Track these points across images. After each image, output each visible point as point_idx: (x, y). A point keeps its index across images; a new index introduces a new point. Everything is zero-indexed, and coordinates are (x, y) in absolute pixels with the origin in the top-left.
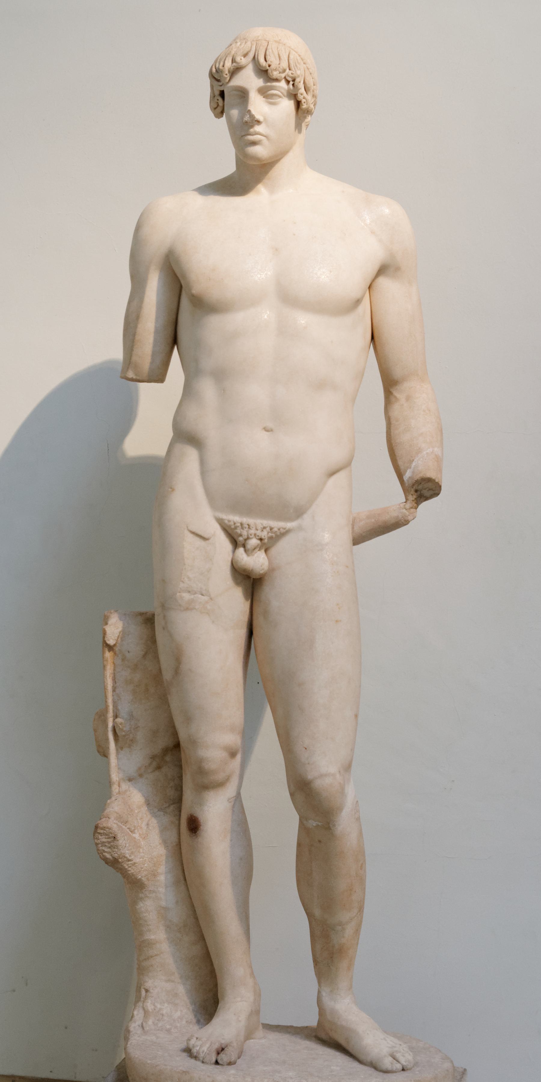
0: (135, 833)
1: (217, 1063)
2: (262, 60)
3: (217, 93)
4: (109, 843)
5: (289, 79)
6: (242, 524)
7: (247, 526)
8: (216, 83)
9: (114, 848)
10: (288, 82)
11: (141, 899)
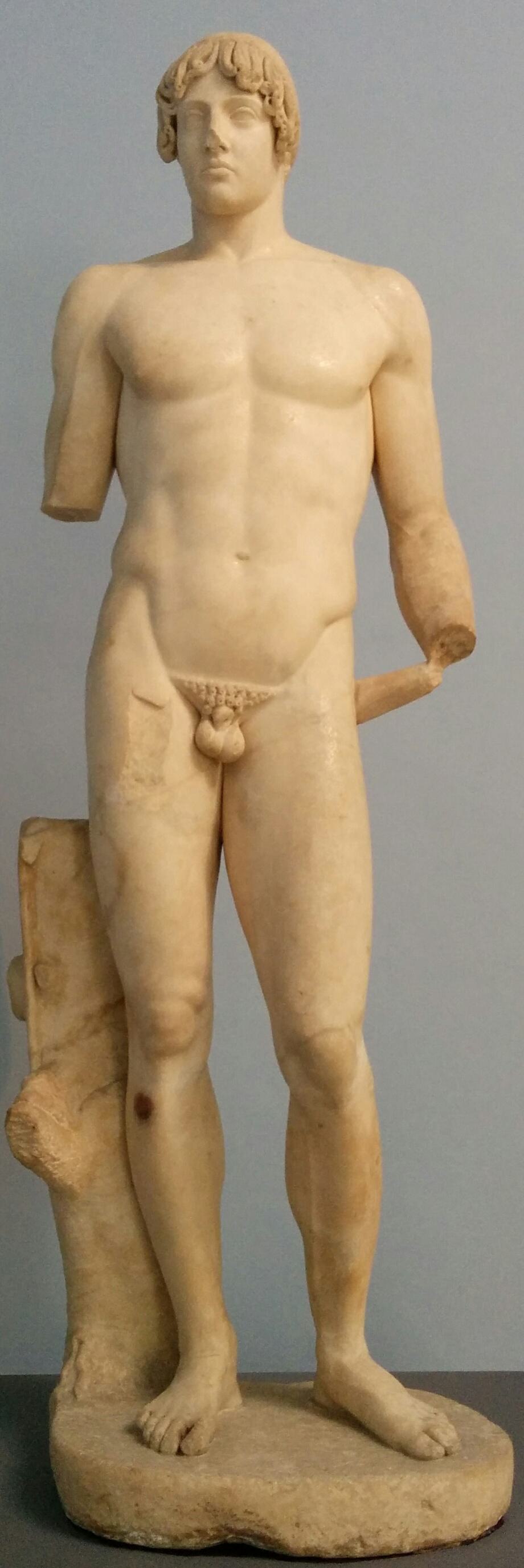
0: (62, 1121)
1: (180, 1452)
2: (227, 61)
3: (167, 120)
5: (264, 92)
6: (207, 687)
7: (215, 691)
8: (165, 105)
10: (263, 97)
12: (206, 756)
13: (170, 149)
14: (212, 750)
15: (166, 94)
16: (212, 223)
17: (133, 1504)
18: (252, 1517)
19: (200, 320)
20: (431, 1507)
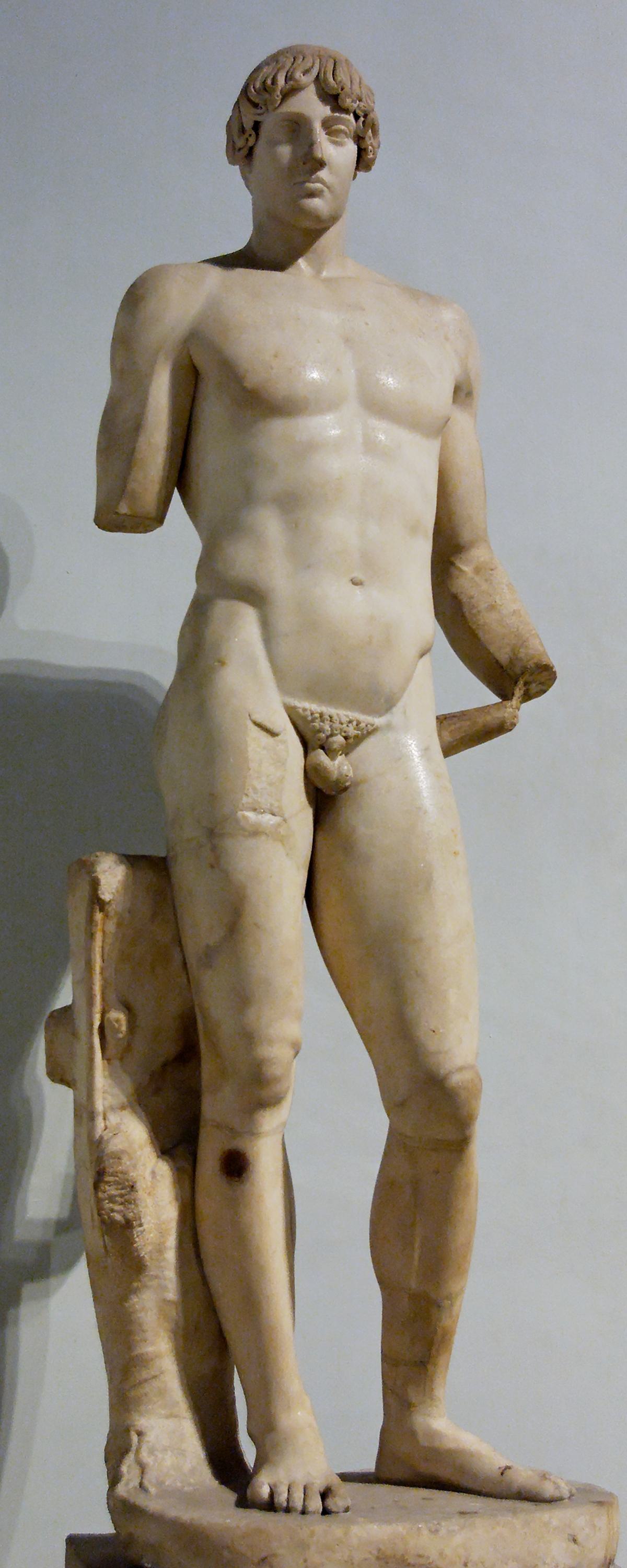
1: (326, 1512)
3: (248, 125)
4: (122, 1196)
8: (246, 108)
9: (130, 1203)
10: (357, 117)
11: (135, 1291)
17: (302, 1561)
18: (422, 1561)
20: (575, 1541)
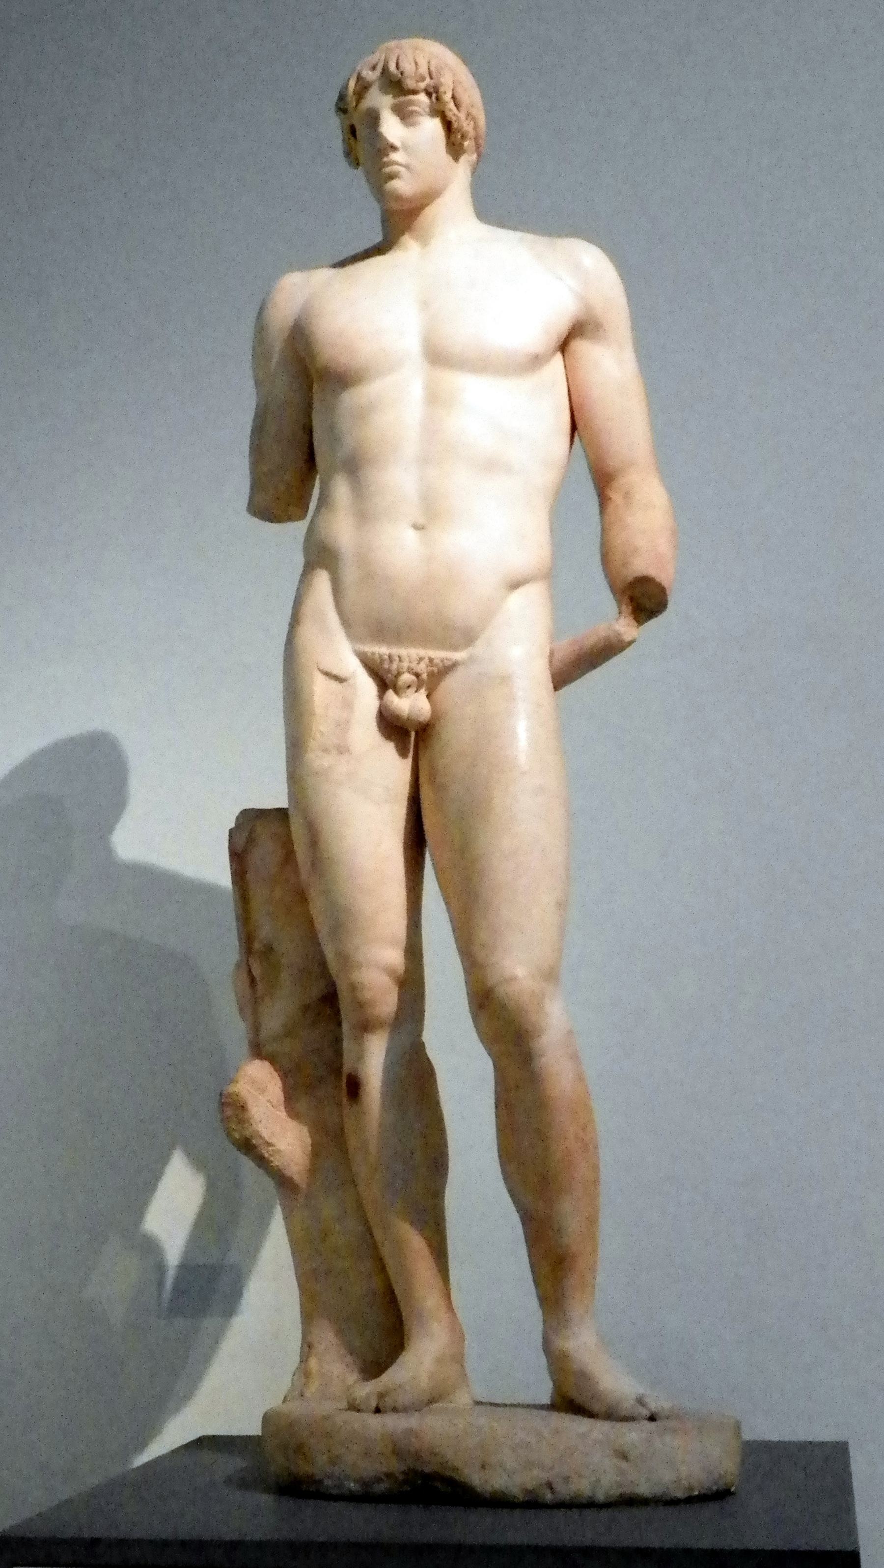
2: (392, 67)
5: (431, 90)
7: (397, 658)
10: (429, 95)
12: (393, 727)
13: (352, 157)
14: (398, 717)
15: (342, 106)
16: (399, 223)
19: (372, 312)
20: (624, 1457)
